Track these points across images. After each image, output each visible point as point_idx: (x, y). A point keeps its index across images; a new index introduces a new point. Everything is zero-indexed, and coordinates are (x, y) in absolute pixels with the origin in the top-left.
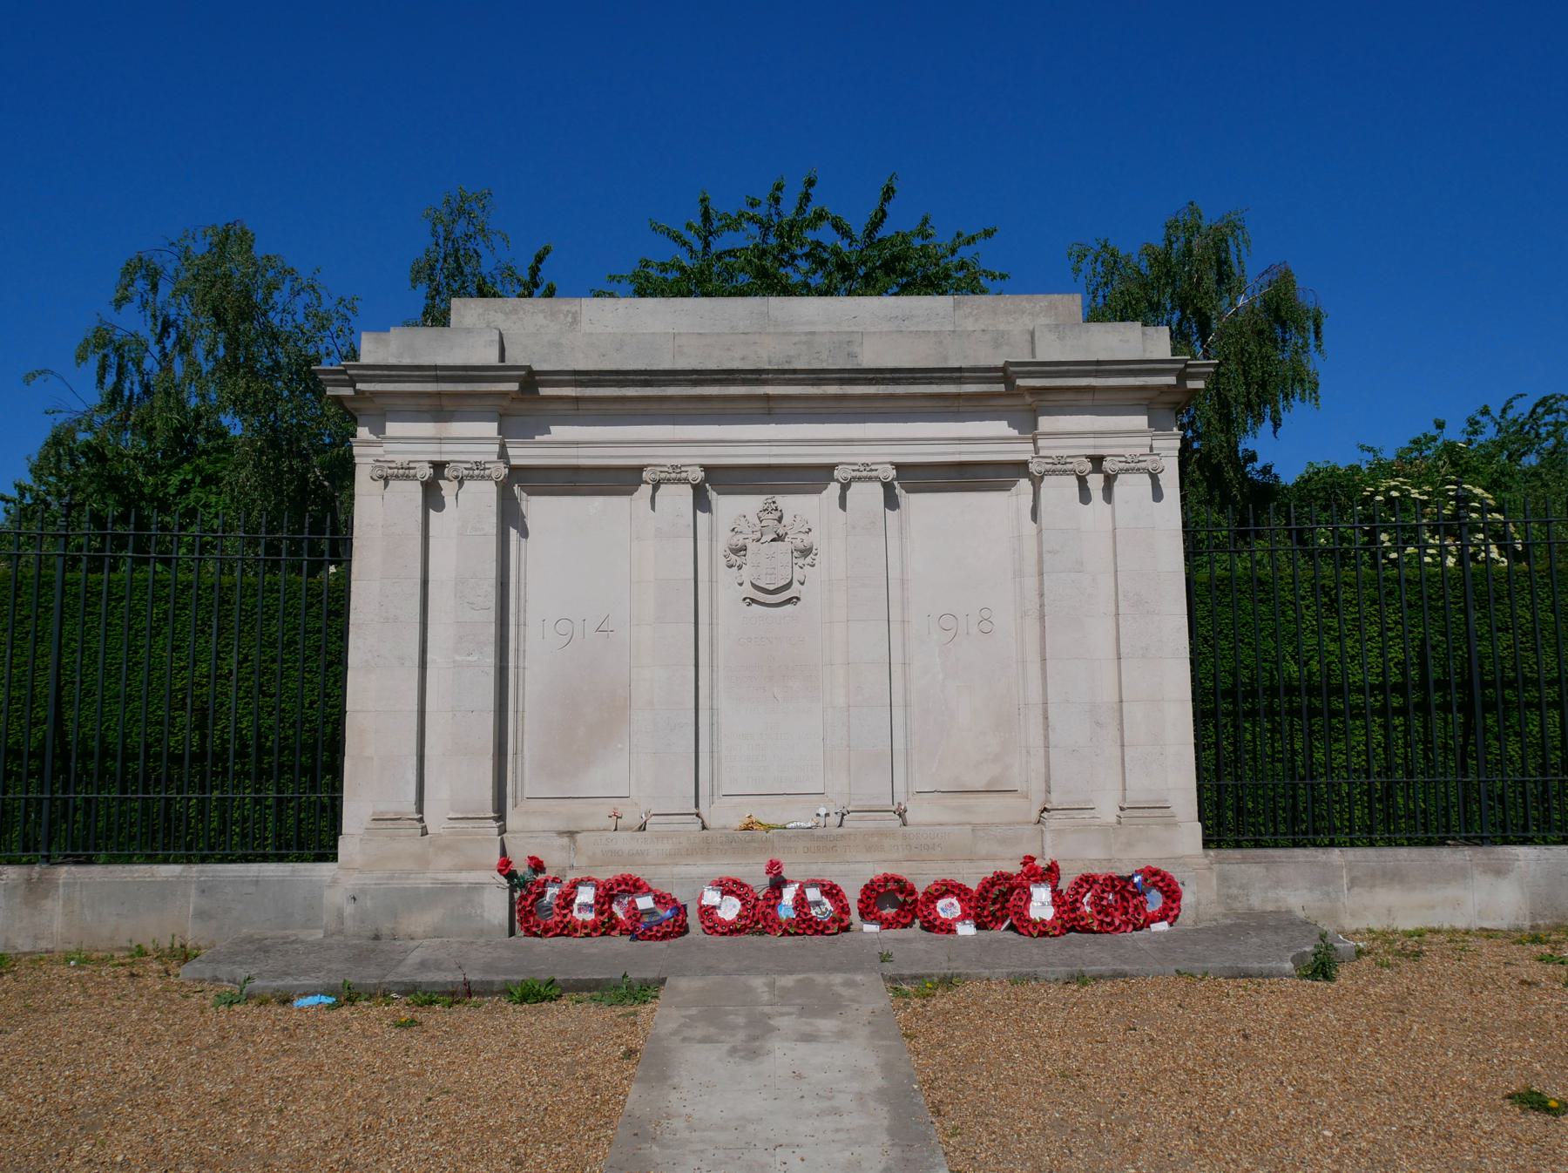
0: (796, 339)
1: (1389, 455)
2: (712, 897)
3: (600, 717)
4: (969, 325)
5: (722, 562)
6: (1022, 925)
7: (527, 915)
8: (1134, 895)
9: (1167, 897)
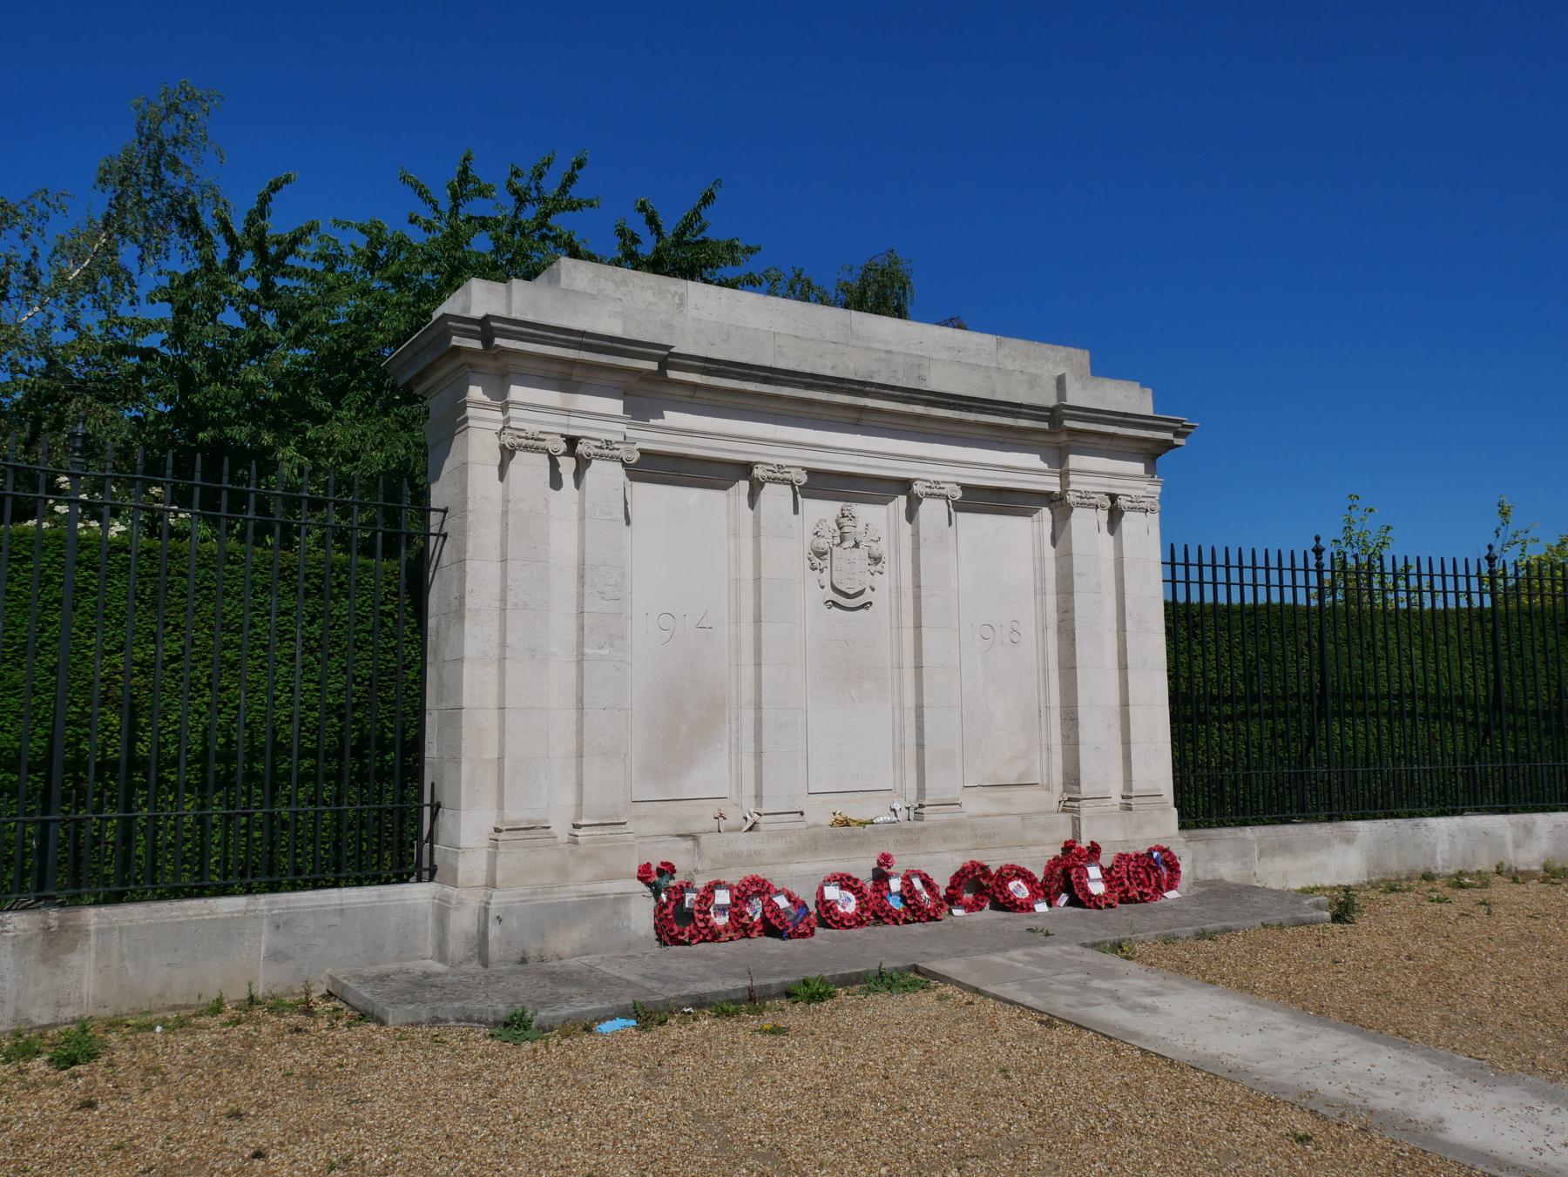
4: (1009, 364)
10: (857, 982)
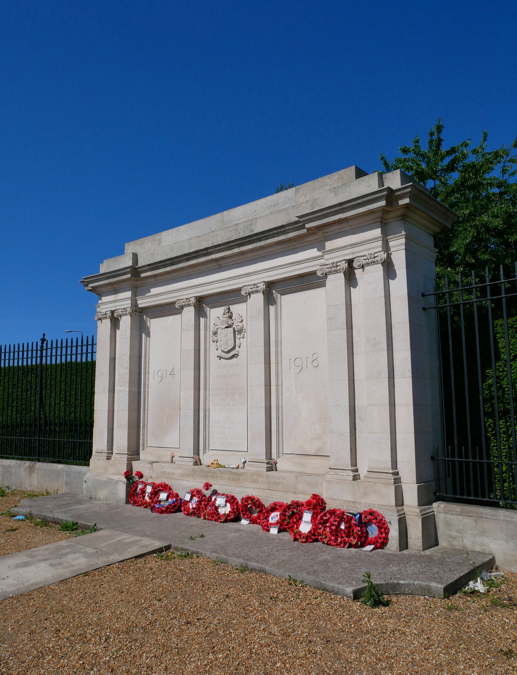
0: (231, 229)
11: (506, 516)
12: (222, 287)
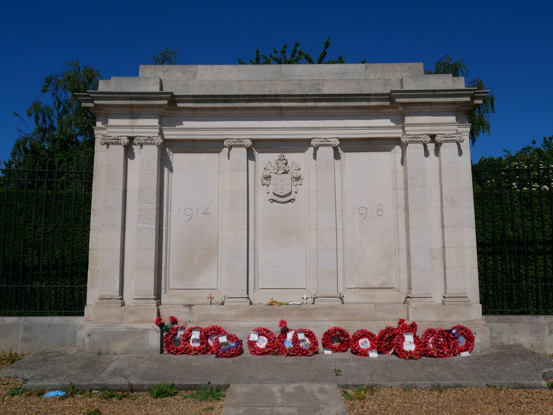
0: (294, 83)
1: (513, 154)
2: (254, 337)
3: (204, 252)
4: (372, 76)
5: (260, 183)
6: (400, 353)
7: (169, 344)
8: (453, 339)
9: (468, 340)
10: (195, 389)
11: (528, 319)
12: (284, 135)
